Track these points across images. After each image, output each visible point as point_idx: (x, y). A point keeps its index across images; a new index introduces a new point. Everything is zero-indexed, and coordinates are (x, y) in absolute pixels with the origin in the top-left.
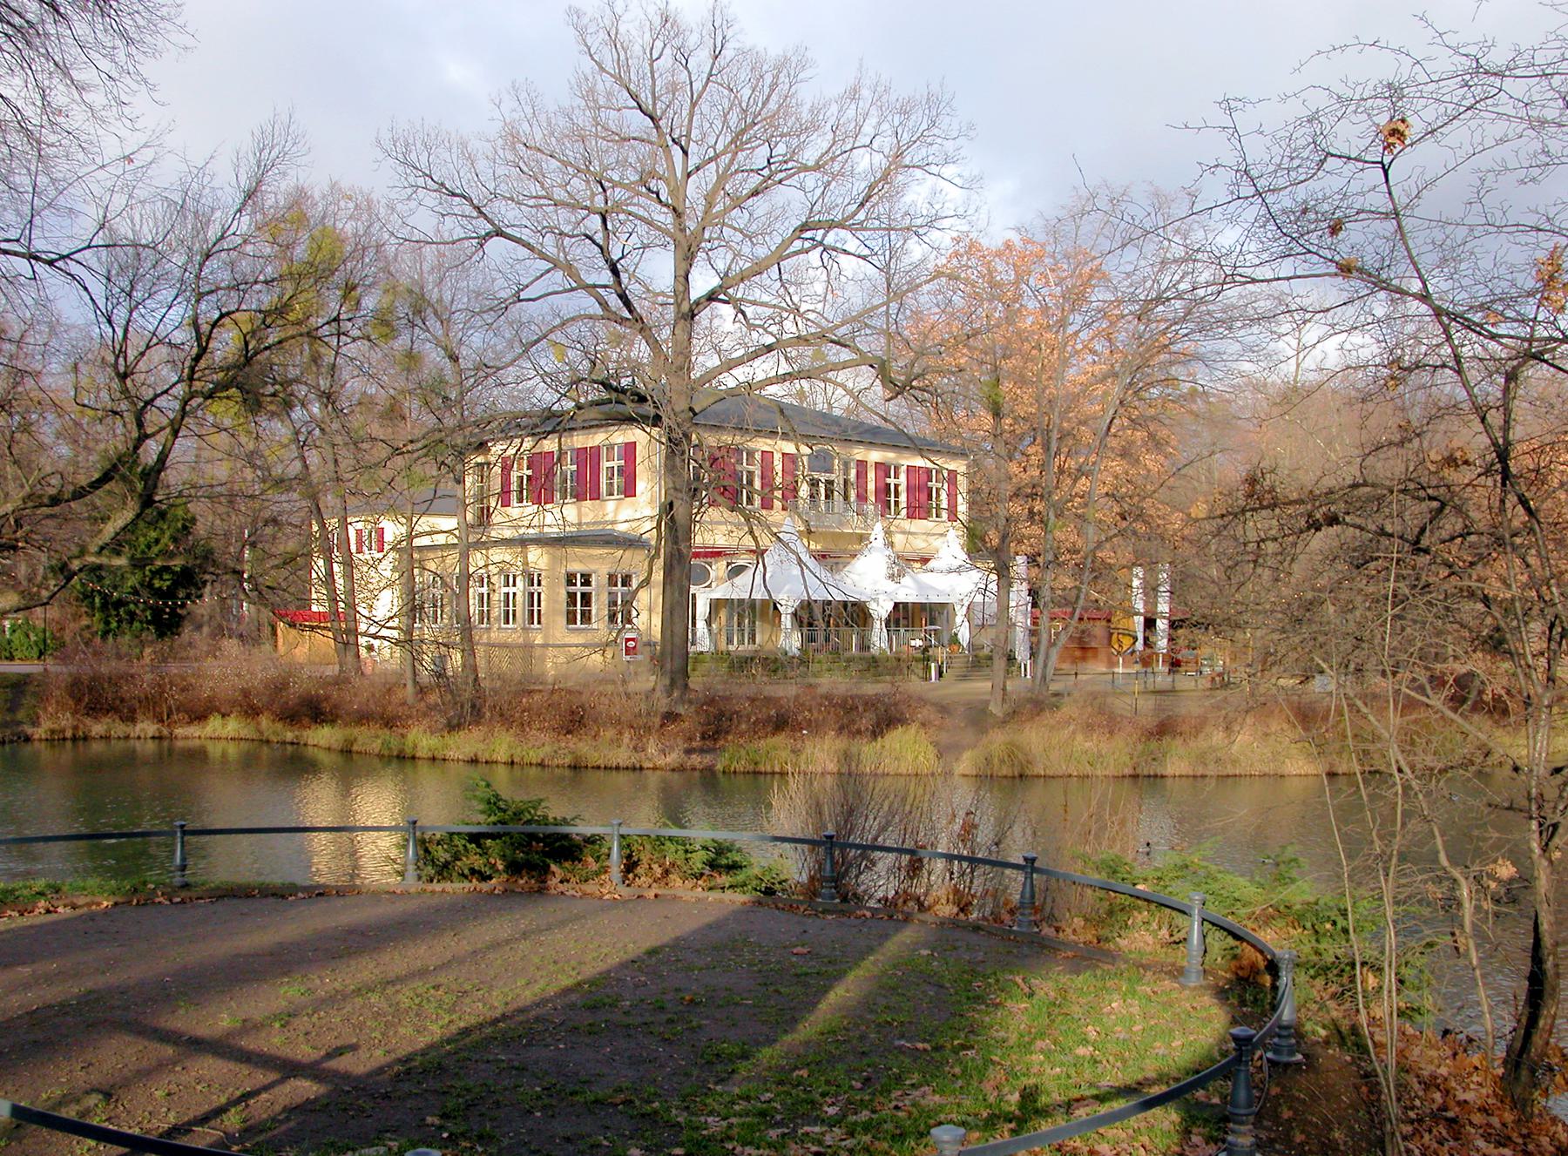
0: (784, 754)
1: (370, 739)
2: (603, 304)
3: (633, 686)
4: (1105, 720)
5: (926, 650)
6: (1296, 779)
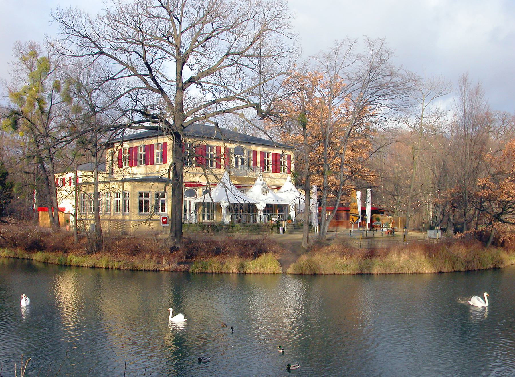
0: (216, 265)
1: (54, 258)
2: (146, 83)
3: (159, 237)
4: (347, 249)
5: (278, 222)
6: (426, 275)
